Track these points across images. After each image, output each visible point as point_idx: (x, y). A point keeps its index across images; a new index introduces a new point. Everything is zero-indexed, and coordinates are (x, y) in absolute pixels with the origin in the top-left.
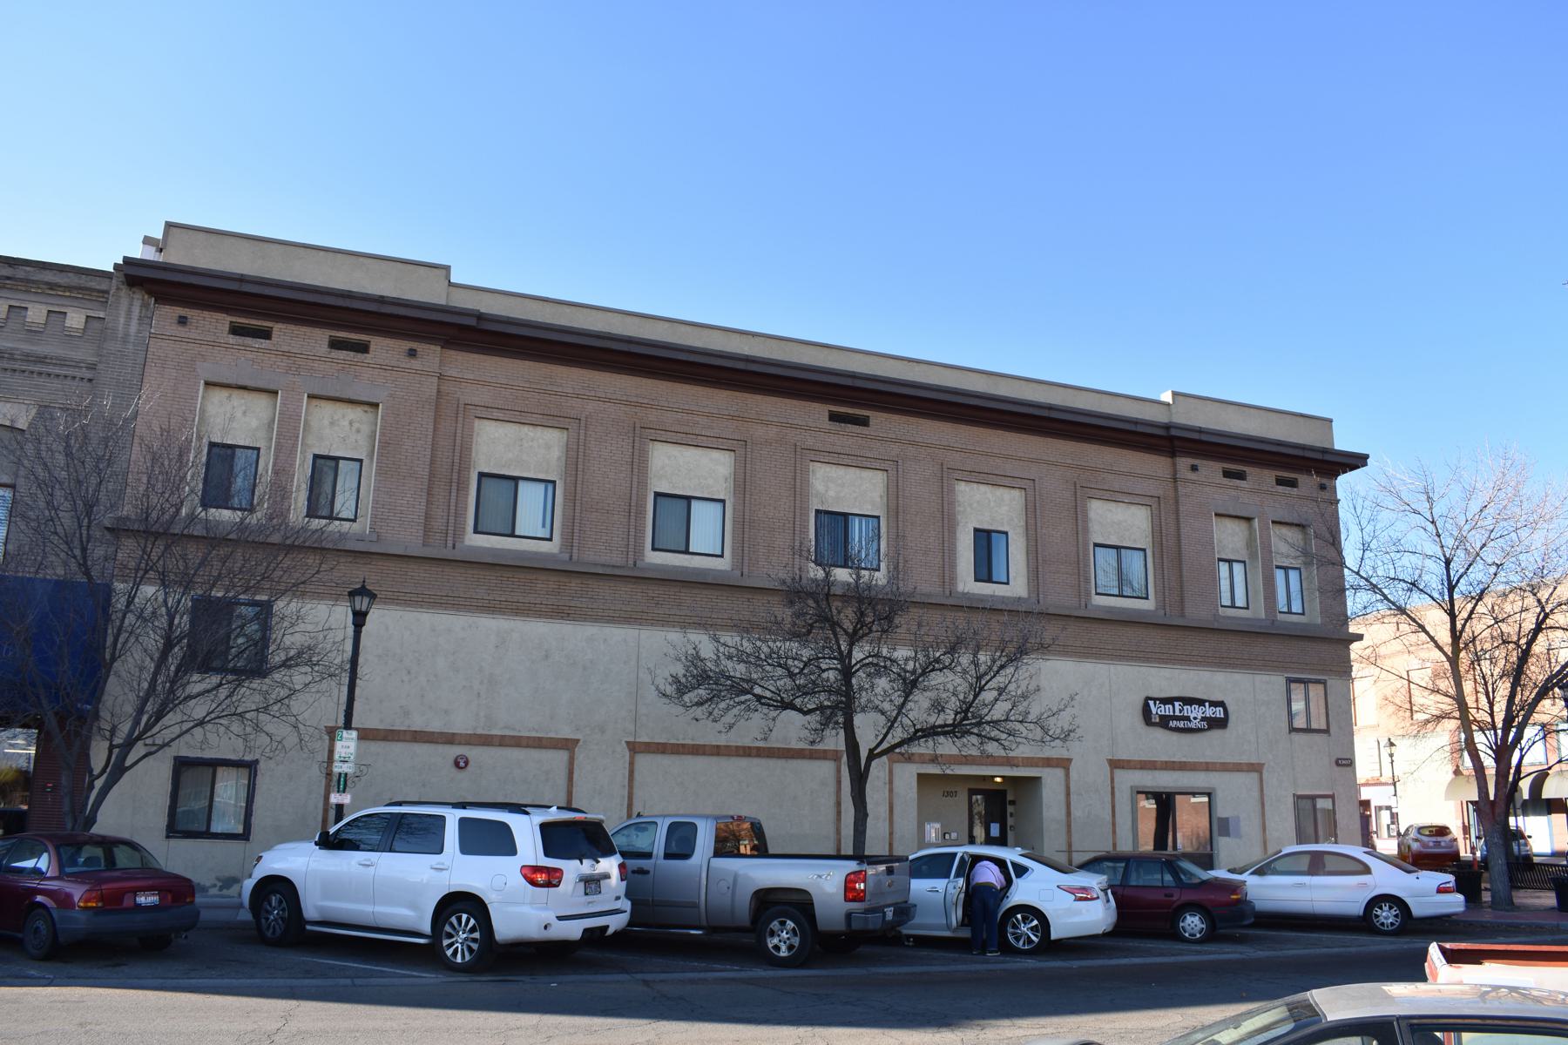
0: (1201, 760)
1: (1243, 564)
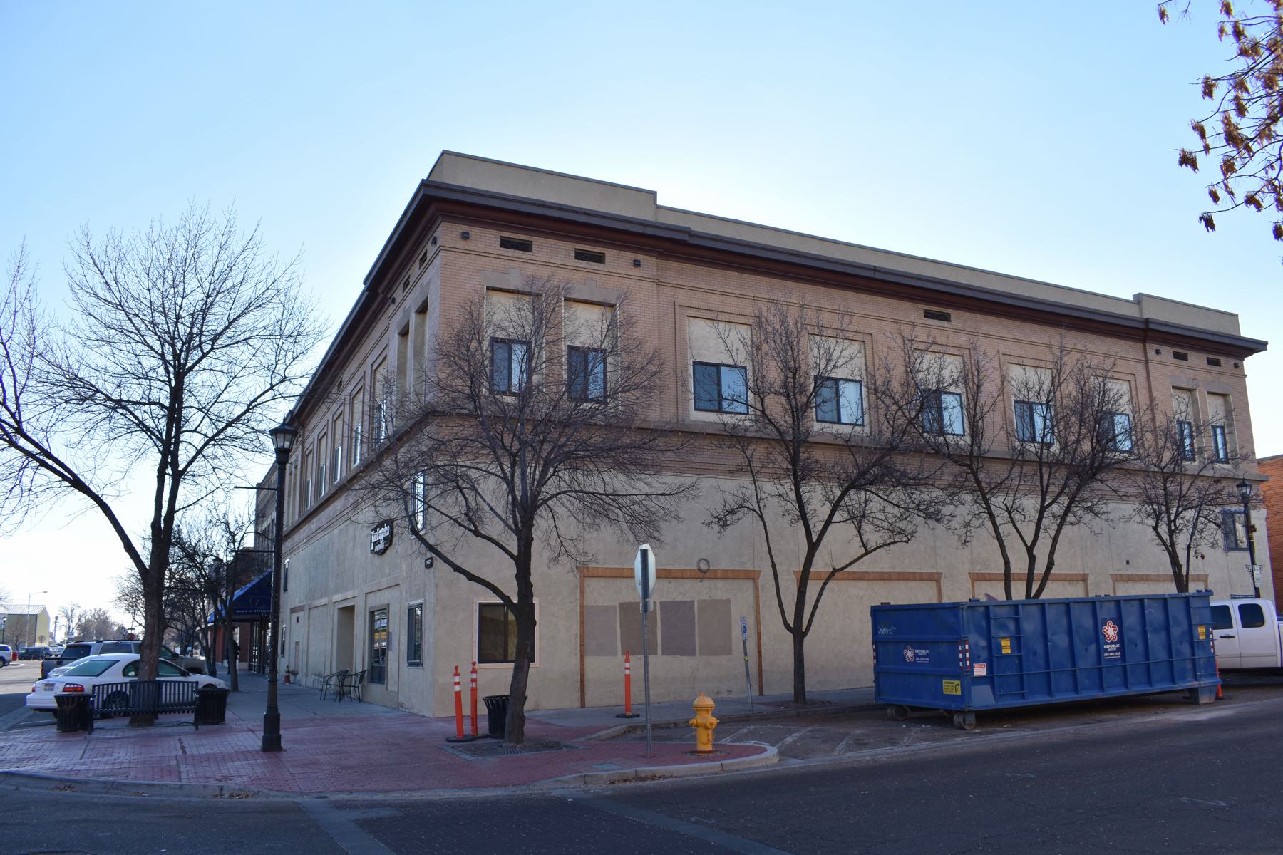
1: (858, 385)
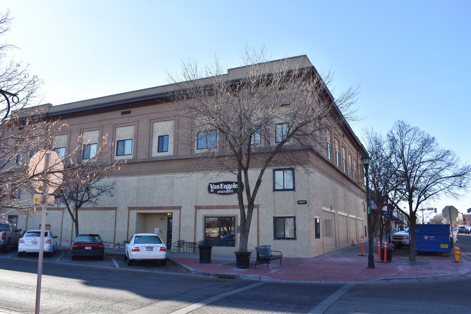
0: (231, 205)
